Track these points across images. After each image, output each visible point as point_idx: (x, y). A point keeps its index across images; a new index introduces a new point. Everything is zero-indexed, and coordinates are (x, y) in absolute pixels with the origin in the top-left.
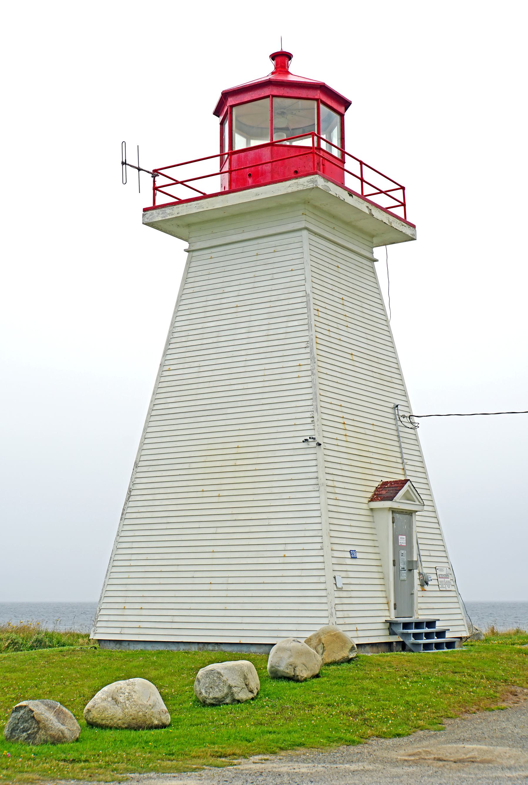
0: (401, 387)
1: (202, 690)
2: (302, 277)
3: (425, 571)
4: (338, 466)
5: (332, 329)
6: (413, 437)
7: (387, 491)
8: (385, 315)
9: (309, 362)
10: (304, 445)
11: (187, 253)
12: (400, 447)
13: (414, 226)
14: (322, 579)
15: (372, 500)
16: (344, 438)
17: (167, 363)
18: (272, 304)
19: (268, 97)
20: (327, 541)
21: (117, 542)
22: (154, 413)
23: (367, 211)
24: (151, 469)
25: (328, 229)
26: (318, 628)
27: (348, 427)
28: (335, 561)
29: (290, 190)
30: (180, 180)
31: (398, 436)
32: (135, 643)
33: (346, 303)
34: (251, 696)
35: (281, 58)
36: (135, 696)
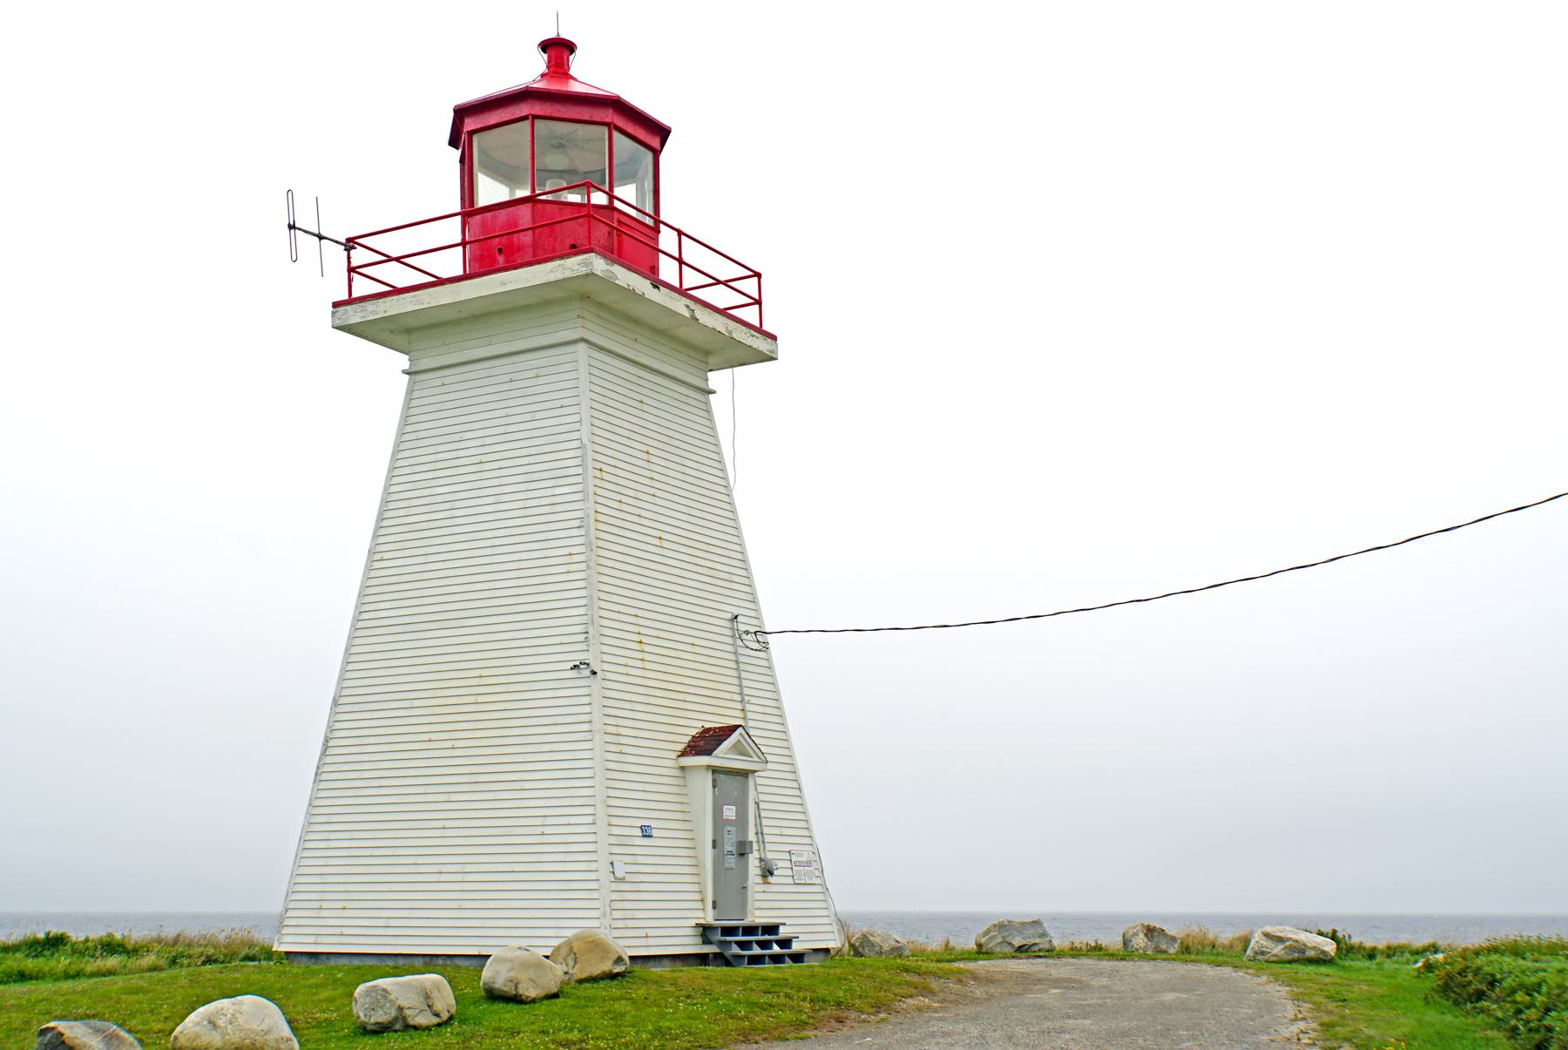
0: (748, 589)
1: (360, 1012)
2: (577, 418)
3: (770, 856)
4: (627, 705)
5: (624, 499)
6: (765, 663)
7: (707, 741)
8: (726, 478)
9: (583, 549)
10: (574, 673)
12: (739, 678)
13: (774, 338)
14: (593, 866)
15: (683, 754)
16: (639, 664)
17: (379, 548)
18: (532, 460)
19: (524, 118)
20: (601, 812)
21: (309, 814)
22: (360, 625)
23: (686, 313)
24: (356, 708)
25: (625, 341)
26: (570, 933)
27: (647, 648)
28: (613, 840)
29: (552, 278)
31: (737, 662)
33: (653, 459)
34: (436, 1020)
35: (558, 50)
36: (241, 1019)
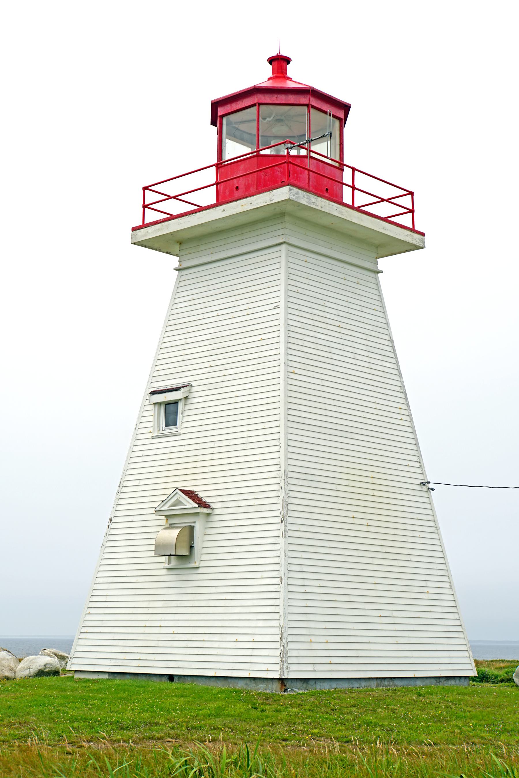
11: (177, 272)
13: (423, 234)
30: (172, 195)
32: (322, 681)
35: (280, 63)
